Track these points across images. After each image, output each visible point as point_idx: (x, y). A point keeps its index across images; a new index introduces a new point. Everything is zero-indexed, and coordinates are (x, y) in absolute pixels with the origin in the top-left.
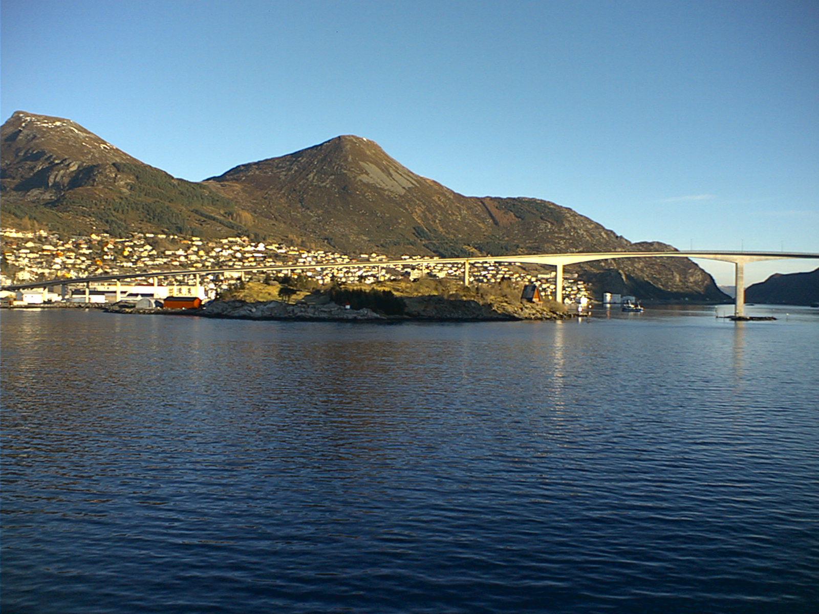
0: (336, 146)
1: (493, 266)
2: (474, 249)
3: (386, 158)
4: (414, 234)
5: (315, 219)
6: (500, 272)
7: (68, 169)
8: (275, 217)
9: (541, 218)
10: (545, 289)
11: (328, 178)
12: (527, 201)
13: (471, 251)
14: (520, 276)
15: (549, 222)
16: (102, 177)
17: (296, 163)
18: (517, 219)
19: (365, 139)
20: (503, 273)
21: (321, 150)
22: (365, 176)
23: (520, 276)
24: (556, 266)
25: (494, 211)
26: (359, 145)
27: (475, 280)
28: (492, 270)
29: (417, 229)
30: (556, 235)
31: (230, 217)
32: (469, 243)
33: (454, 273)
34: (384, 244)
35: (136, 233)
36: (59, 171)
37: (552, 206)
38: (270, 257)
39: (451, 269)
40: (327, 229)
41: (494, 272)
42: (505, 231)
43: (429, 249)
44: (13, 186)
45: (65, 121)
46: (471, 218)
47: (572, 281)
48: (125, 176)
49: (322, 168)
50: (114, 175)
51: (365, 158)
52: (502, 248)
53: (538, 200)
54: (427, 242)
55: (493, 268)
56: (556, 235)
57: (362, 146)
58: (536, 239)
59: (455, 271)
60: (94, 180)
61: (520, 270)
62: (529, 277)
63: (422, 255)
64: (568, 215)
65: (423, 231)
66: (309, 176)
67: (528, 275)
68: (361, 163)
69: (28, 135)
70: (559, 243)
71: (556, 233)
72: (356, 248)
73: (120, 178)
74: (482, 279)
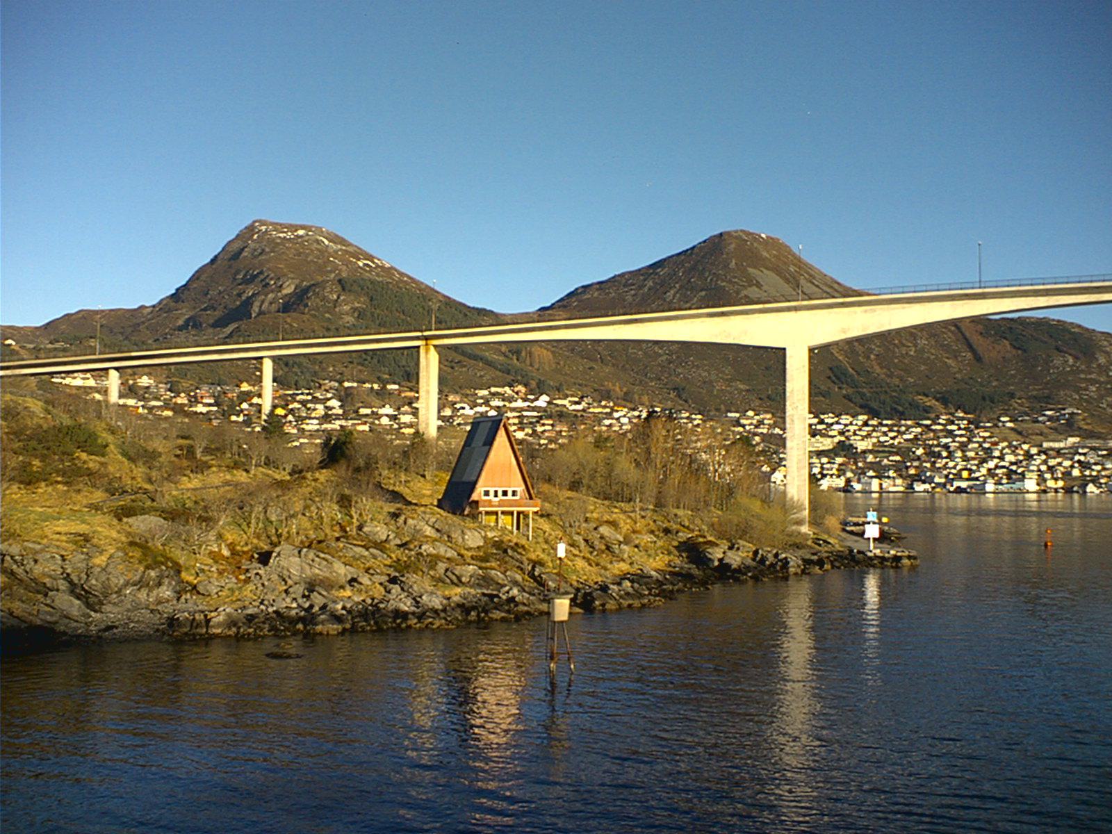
0: (716, 244)
1: (964, 429)
2: (934, 401)
3: (795, 261)
4: (829, 378)
5: (664, 358)
6: (975, 440)
7: (280, 291)
8: (601, 358)
9: (1058, 349)
10: (1053, 467)
11: (695, 296)
12: (1033, 323)
13: (928, 404)
14: (1009, 447)
15: (1070, 355)
16: (318, 300)
17: (652, 276)
18: (1014, 352)
19: (763, 236)
20: (981, 440)
21: (692, 253)
22: (755, 288)
23: (1009, 447)
24: (784, 349)
25: (977, 340)
26: (752, 244)
27: (925, 453)
28: (961, 436)
29: (835, 369)
30: (1082, 376)
31: (515, 357)
32: (926, 392)
33: (891, 442)
34: (774, 396)
35: (327, 381)
36: (266, 296)
37: (1076, 330)
38: (550, 417)
39: (885, 434)
40: (679, 374)
41: (965, 439)
42: (992, 371)
43: (852, 402)
44: (211, 321)
45: (313, 229)
46: (933, 351)
47: (1105, 452)
48: (352, 297)
49: (689, 281)
50: (335, 297)
51: (757, 261)
52: (984, 399)
53: (1053, 320)
54: (850, 391)
55: (963, 432)
56: (1082, 376)
57: (755, 245)
58: (1047, 383)
59: (893, 438)
60: (306, 305)
61: (1013, 435)
62: (1025, 447)
63: (837, 412)
64: (1105, 343)
65: (845, 373)
66: (668, 294)
67: (1024, 443)
68: (751, 270)
69: (255, 250)
70: (1086, 389)
71: (1082, 371)
72: (723, 402)
73: (344, 300)
74: (939, 452)
